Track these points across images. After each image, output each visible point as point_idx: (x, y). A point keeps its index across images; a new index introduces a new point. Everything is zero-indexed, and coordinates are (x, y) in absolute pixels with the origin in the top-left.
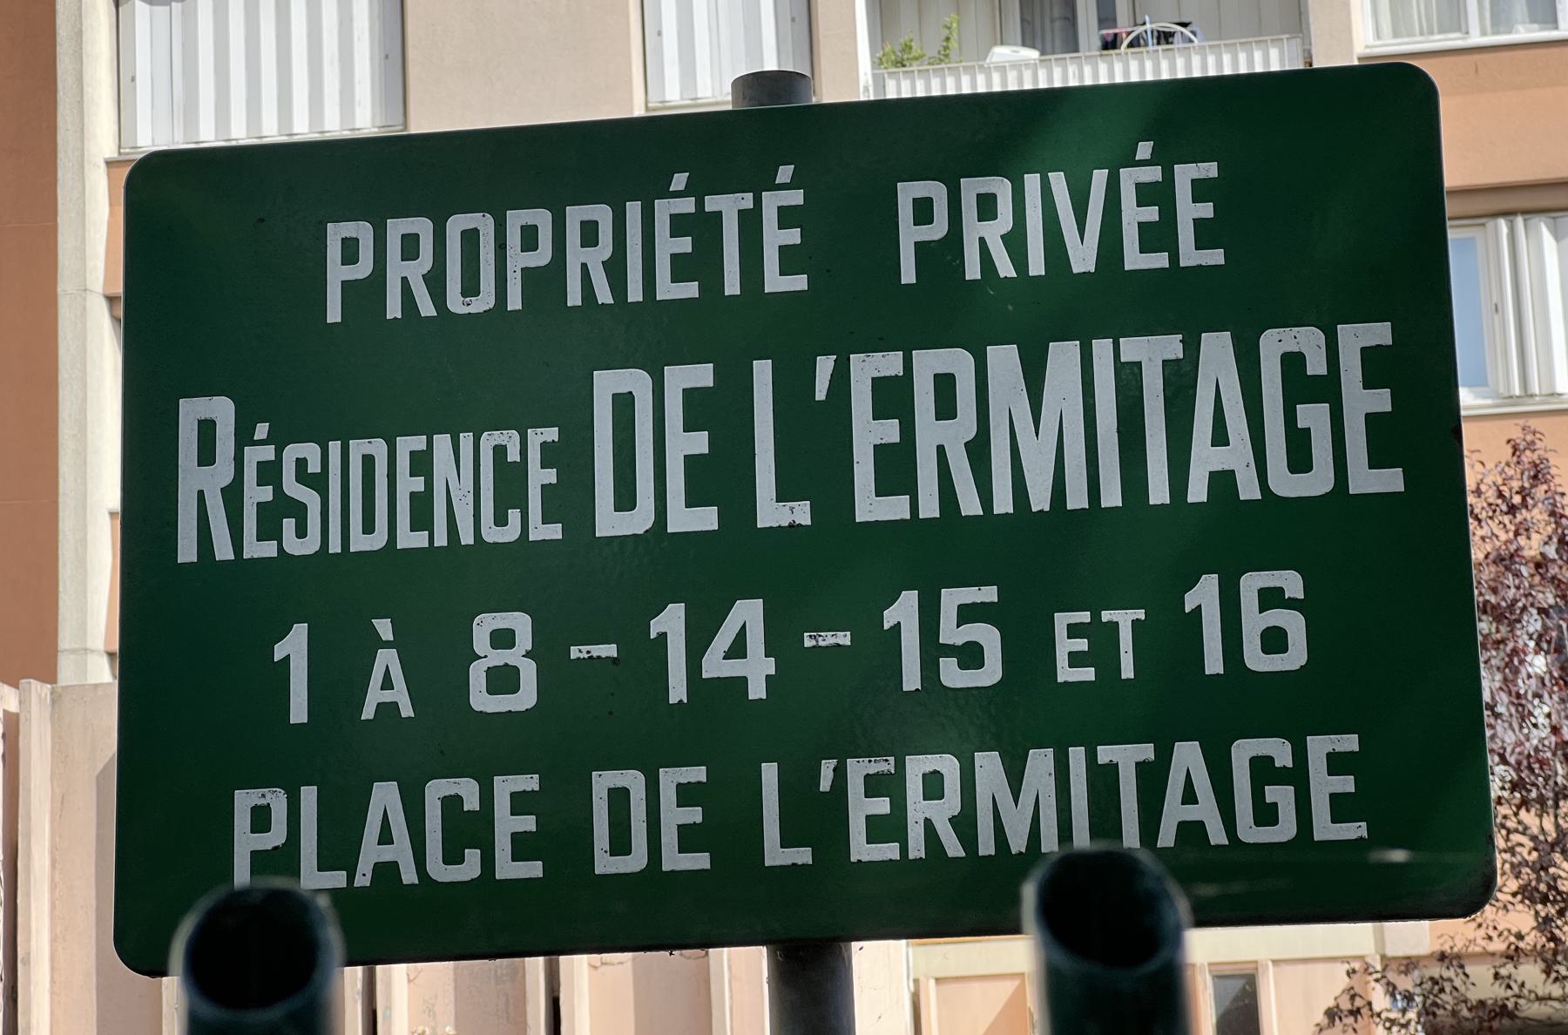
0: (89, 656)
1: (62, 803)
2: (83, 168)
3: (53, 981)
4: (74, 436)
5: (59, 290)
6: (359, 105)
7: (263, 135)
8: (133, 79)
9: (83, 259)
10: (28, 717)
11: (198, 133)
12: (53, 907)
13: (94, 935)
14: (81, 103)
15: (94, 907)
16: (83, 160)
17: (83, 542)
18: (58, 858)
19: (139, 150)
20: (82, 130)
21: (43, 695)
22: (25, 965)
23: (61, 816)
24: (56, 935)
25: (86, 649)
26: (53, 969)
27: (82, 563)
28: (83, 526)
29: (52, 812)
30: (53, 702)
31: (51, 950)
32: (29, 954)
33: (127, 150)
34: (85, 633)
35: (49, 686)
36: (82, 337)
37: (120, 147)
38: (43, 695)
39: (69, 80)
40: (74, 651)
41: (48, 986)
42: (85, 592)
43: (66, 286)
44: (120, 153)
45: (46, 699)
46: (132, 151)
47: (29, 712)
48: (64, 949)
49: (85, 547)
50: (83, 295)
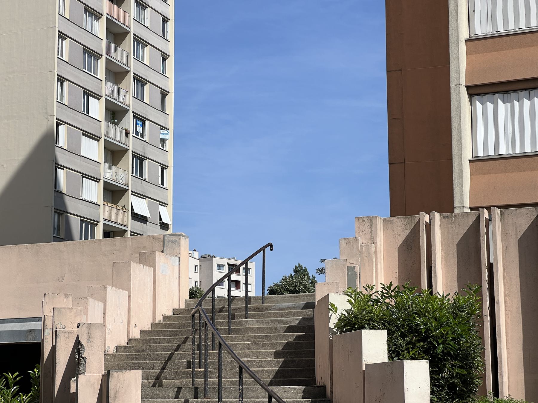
0: (465, 209)
1: (506, 249)
2: (458, 42)
3: (506, 310)
4: (457, 134)
5: (451, 85)
6: (147, 77)
7: (521, 28)
8: (474, 11)
9: (459, 74)
10: (495, 220)
11: (497, 29)
12: (504, 285)
13: (520, 295)
14: (457, 20)
15: (519, 285)
16: (458, 40)
17: (461, 170)
18: (506, 268)
19: (521, 29)
20: (458, 29)
21: (498, 213)
22: (497, 304)
23: (506, 254)
24: (506, 294)
25: (464, 207)
26: (505, 306)
27: (461, 177)
28: (461, 165)
29: (503, 252)
30: (501, 215)
31: (505, 300)
32: (499, 300)
33: (472, 36)
34: (463, 201)
35: (500, 210)
36: (459, 100)
37: (469, 35)
38: (498, 213)
39: (453, 12)
40: (459, 207)
41: (504, 312)
42: (462, 187)
43: (453, 83)
44: (469, 37)
45: (499, 214)
46: (519, 30)
47: (495, 218)
48: (509, 299)
49: (462, 172)
50: (459, 86)
